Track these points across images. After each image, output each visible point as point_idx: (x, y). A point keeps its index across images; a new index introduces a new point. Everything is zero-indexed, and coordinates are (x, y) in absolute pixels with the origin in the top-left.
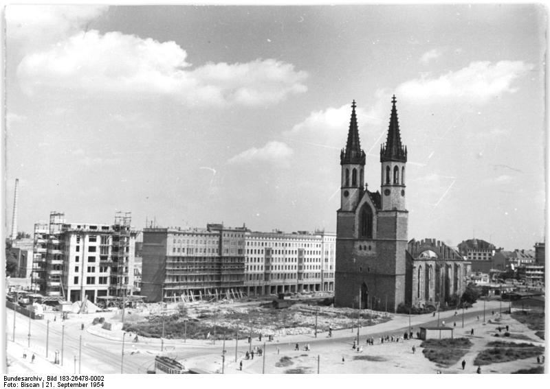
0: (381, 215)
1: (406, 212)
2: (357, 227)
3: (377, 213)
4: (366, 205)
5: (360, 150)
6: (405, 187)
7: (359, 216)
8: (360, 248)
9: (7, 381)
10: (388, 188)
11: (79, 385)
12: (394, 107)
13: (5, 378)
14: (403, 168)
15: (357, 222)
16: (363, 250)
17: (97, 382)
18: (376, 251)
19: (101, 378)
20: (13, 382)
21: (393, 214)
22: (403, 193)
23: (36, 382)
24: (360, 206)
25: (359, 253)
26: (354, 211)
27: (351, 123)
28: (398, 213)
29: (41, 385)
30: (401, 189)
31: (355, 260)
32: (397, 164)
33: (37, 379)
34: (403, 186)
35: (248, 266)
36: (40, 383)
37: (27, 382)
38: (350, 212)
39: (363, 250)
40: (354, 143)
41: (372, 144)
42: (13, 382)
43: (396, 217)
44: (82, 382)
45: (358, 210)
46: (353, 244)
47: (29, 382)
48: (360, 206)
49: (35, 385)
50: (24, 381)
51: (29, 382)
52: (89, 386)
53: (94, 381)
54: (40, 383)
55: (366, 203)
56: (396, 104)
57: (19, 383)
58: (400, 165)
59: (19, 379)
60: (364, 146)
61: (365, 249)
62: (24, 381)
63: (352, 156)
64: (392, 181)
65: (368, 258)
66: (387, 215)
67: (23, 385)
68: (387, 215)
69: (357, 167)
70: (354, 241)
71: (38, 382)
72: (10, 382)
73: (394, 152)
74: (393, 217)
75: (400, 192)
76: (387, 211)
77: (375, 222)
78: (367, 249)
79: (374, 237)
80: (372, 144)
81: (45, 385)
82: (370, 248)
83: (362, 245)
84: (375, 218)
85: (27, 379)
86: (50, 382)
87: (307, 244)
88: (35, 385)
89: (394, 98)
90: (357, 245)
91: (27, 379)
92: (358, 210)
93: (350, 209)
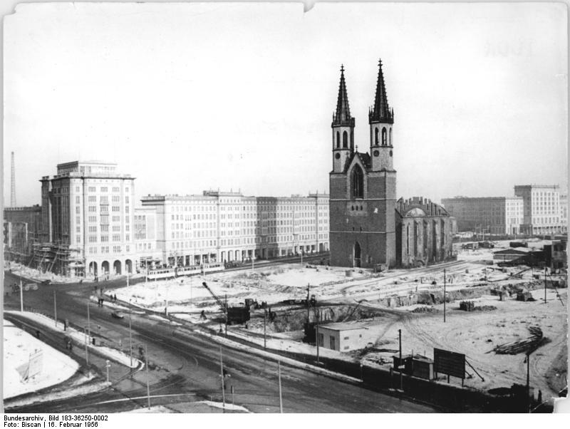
0: (371, 175)
1: (395, 172)
2: (349, 188)
4: (357, 165)
7: (351, 177)
8: (353, 208)
10: (377, 149)
12: (380, 70)
13: (6, 418)
15: (349, 183)
16: (355, 210)
20: (14, 422)
21: (382, 174)
23: (37, 422)
25: (352, 213)
26: (345, 172)
28: (387, 174)
29: (42, 425)
30: (389, 149)
31: (347, 220)
33: (38, 419)
34: (391, 147)
36: (42, 422)
37: (28, 422)
38: (342, 173)
39: (355, 210)
41: (361, 107)
42: (14, 422)
45: (349, 171)
47: (30, 422)
48: (351, 167)
49: (36, 425)
50: (25, 421)
51: (30, 422)
54: (42, 422)
55: (357, 165)
56: (382, 67)
58: (387, 126)
59: (20, 418)
60: (354, 113)
62: (25, 421)
63: (343, 118)
64: (381, 143)
65: (360, 217)
66: (376, 175)
67: (23, 425)
68: (376, 175)
69: (348, 129)
71: (40, 422)
72: (10, 422)
73: (381, 114)
76: (376, 172)
77: (365, 183)
78: (359, 209)
80: (361, 107)
81: (47, 424)
82: (362, 208)
84: (365, 178)
85: (28, 419)
86: (51, 422)
87: (355, 206)
88: (36, 425)
89: (342, 67)
90: (349, 206)
91: (28, 419)
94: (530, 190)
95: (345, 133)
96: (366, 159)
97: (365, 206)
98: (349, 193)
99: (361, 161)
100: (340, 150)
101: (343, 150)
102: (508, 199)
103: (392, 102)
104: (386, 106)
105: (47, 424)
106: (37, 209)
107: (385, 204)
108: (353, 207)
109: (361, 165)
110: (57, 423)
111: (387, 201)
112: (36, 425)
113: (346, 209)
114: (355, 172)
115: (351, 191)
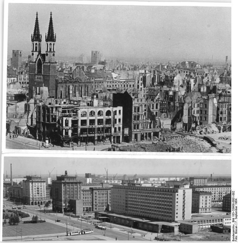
0: (45, 64)
2: (36, 69)
3: (43, 63)
4: (40, 59)
5: (39, 34)
6: (55, 52)
7: (37, 64)
9: (235, 240)
11: (236, 209)
13: (233, 241)
14: (54, 44)
17: (235, 202)
18: (43, 80)
19: (233, 192)
20: (235, 237)
21: (49, 64)
22: (54, 55)
23: (235, 227)
24: (37, 60)
27: (50, 22)
28: (51, 64)
29: (236, 225)
30: (53, 53)
31: (35, 83)
32: (51, 42)
33: (234, 227)
34: (54, 52)
35: (157, 108)
36: (235, 225)
37: (235, 231)
38: (34, 62)
40: (36, 32)
41: (44, 32)
42: (235, 237)
43: (50, 65)
44: (235, 208)
45: (37, 61)
46: (35, 76)
47: (235, 230)
48: (37, 60)
49: (236, 228)
50: (235, 232)
51: (235, 230)
52: (236, 205)
53: (234, 201)
54: (235, 225)
55: (40, 59)
57: (235, 235)
58: (52, 43)
59: (233, 235)
61: (39, 79)
63: (36, 37)
66: (47, 64)
67: (236, 233)
68: (47, 64)
69: (37, 42)
70: (35, 75)
71: (235, 226)
72: (235, 239)
73: (51, 37)
74: (48, 65)
75: (52, 55)
76: (47, 63)
77: (42, 67)
79: (42, 74)
80: (44, 32)
81: (236, 223)
83: (38, 77)
84: (43, 65)
85: (234, 231)
90: (36, 77)
91: (234, 231)
92: (37, 61)
93: (34, 61)
94: (45, 65)
95: (36, 44)
96: (44, 56)
97: (42, 78)
98: (36, 71)
99: (41, 57)
100: (34, 52)
101: (35, 52)
102: (197, 91)
103: (55, 31)
104: (53, 34)
105: (236, 223)
106: (187, 124)
107: (49, 77)
108: (38, 77)
109: (41, 59)
110: (235, 220)
111: (50, 76)
112: (236, 228)
113: (35, 78)
114: (39, 62)
115: (37, 70)
